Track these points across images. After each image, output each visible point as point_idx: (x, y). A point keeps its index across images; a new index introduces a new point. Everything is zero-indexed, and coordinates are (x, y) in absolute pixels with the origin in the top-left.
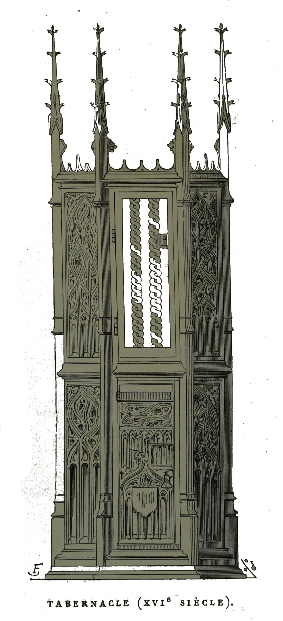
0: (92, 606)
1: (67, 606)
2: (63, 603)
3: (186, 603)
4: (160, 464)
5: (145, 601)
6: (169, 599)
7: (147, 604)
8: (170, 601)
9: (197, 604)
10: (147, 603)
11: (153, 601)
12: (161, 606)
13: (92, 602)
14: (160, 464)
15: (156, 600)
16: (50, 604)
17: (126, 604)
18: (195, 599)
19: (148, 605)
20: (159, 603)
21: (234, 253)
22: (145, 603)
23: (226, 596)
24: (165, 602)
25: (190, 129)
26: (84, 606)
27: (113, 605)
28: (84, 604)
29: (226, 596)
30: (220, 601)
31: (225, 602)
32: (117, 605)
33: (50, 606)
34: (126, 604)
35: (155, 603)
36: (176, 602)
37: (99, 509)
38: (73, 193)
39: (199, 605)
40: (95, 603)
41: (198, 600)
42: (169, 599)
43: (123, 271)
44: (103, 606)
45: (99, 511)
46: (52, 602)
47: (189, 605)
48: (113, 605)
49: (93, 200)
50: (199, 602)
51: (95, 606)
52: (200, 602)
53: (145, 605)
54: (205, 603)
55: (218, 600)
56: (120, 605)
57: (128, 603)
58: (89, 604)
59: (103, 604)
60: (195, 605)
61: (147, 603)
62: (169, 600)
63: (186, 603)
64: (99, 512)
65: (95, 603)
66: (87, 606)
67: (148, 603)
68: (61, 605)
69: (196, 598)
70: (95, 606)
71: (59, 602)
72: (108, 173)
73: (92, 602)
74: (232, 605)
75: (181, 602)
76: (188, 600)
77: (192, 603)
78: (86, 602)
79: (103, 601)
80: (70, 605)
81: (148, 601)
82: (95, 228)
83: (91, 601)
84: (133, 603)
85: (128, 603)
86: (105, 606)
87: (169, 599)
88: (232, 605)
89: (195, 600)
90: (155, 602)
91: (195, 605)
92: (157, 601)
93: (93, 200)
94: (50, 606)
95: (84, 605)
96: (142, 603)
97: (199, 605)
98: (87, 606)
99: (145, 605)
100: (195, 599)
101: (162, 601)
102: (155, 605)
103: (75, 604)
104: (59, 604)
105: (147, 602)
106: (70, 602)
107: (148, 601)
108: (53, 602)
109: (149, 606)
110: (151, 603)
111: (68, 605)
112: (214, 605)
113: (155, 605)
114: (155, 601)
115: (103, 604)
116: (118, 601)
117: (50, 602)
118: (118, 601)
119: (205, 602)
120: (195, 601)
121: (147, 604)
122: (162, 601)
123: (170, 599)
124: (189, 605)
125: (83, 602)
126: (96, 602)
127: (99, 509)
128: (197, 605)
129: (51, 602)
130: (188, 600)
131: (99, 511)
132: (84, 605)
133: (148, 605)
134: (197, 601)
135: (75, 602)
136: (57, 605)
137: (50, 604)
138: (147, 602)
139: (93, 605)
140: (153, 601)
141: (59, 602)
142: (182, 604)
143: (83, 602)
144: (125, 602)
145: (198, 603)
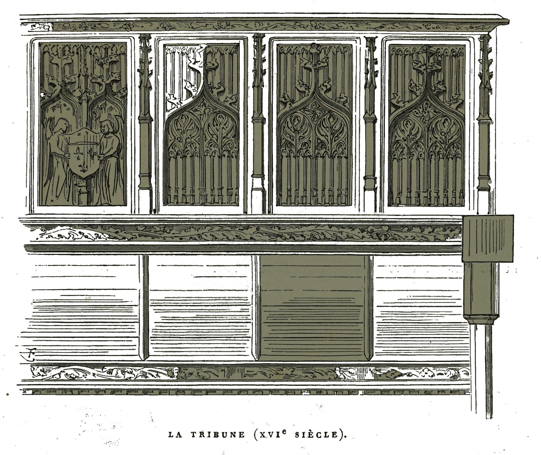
1: (215, 437)
3: (301, 435)
4: (375, 211)
5: (261, 433)
6: (284, 431)
7: (263, 436)
8: (286, 433)
9: (311, 436)
11: (269, 433)
12: (277, 437)
13: (232, 433)
14: (375, 211)
17: (242, 436)
18: (309, 431)
20: (275, 434)
23: (340, 429)
24: (281, 434)
27: (320, 437)
28: (233, 434)
29: (340, 429)
30: (334, 434)
31: (339, 434)
32: (325, 437)
33: (193, 436)
40: (234, 434)
41: (312, 433)
43: (254, 100)
50: (313, 435)
51: (235, 436)
52: (314, 435)
56: (328, 437)
61: (262, 435)
62: (284, 433)
63: (301, 435)
64: (449, 278)
65: (234, 434)
67: (264, 435)
68: (181, 436)
69: (310, 430)
70: (235, 436)
72: (194, 204)
73: (232, 433)
77: (307, 435)
79: (179, 433)
80: (218, 436)
82: (155, 312)
84: (249, 435)
85: (336, 434)
87: (284, 431)
88: (345, 437)
90: (271, 434)
92: (273, 432)
94: (193, 436)
95: (202, 436)
96: (258, 435)
97: (313, 437)
98: (204, 437)
100: (309, 431)
101: (278, 433)
102: (271, 436)
106: (218, 433)
108: (196, 433)
111: (216, 436)
112: (172, 436)
113: (271, 436)
116: (326, 433)
117: (193, 433)
118: (326, 433)
119: (319, 434)
120: (309, 433)
121: (263, 436)
122: (278, 433)
123: (285, 431)
124: (304, 437)
126: (235, 433)
129: (195, 433)
132: (202, 436)
134: (311, 433)
136: (201, 435)
140: (269, 433)
143: (215, 433)
144: (202, 434)
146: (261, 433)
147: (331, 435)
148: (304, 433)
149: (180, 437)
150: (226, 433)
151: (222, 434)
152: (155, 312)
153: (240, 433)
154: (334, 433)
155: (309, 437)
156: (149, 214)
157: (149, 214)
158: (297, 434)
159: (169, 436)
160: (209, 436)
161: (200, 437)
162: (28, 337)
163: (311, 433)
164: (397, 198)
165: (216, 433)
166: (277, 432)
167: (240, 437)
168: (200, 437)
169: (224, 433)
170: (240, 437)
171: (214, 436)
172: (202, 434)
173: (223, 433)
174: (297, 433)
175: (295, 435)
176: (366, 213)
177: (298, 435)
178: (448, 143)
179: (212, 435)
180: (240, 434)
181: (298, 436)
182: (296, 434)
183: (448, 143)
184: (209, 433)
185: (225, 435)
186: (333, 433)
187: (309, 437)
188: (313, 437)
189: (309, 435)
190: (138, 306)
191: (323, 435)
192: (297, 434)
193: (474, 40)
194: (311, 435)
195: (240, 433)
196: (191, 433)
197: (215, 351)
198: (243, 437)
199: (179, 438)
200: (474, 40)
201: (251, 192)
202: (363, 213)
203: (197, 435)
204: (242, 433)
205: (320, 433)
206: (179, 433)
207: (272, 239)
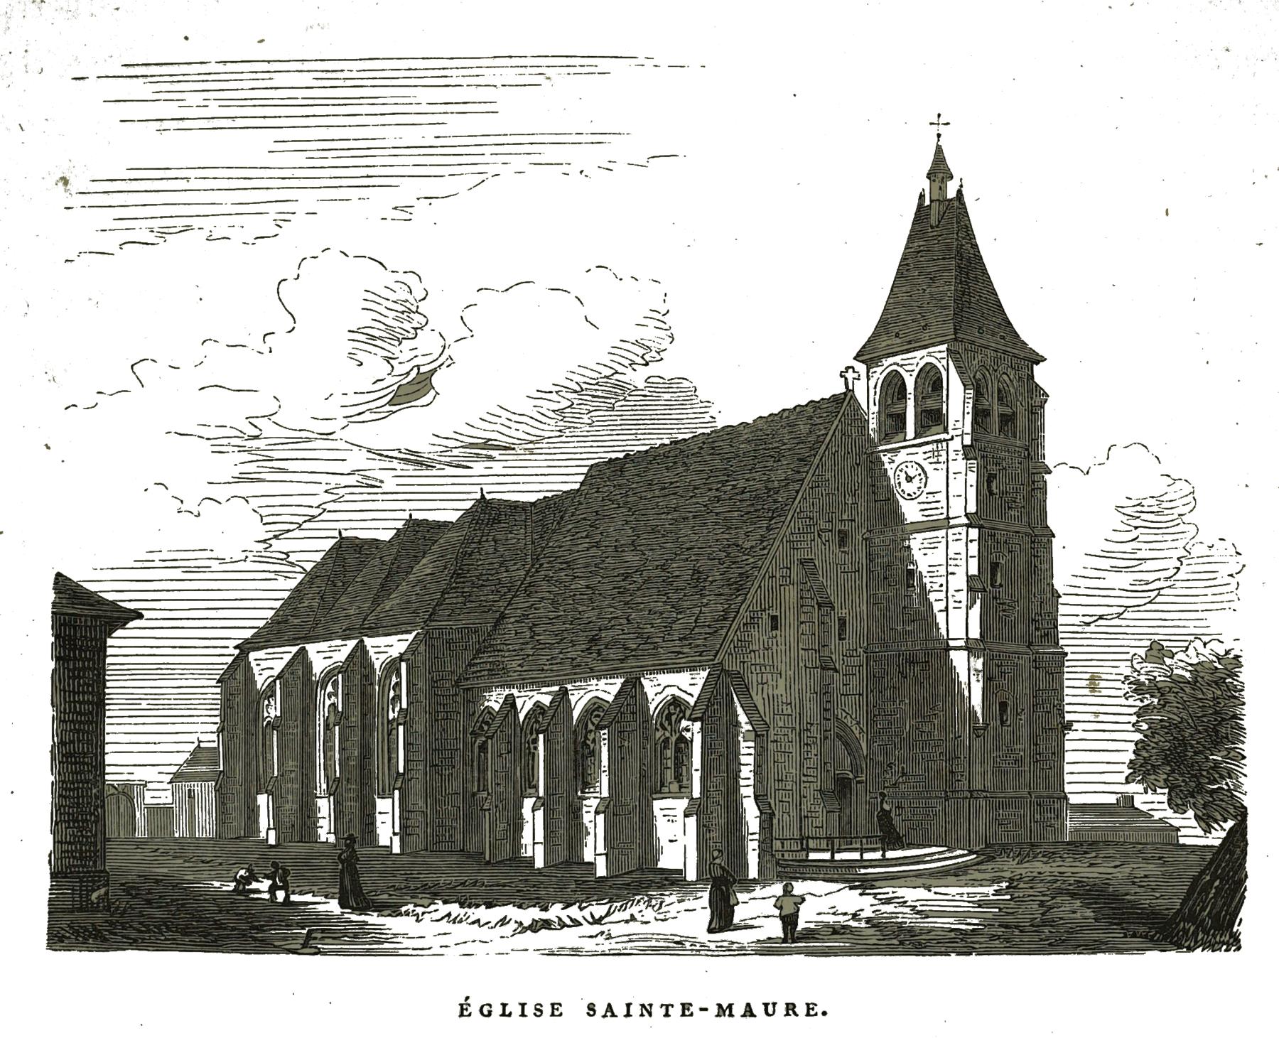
0: (642, 1015)
2: (758, 1009)
13: (643, 1006)
15: (771, 1002)
16: (667, 1010)
17: (687, 1013)
28: (791, 1008)
32: (503, 1015)
33: (667, 1015)
37: (294, 318)
39: (470, 1015)
44: (750, 1016)
45: (173, 434)
46: (672, 1006)
51: (650, 1014)
52: (474, 1009)
55: (682, 1004)
56: (510, 1015)
57: (815, 1007)
58: (801, 1009)
64: (176, 433)
65: (648, 1007)
66: (796, 1015)
70: (650, 1014)
71: (748, 1005)
73: (643, 1006)
78: (794, 1006)
79: (609, 1005)
83: (718, 1005)
85: (692, 1009)
86: (753, 1015)
95: (791, 1012)
98: (796, 1015)
104: (749, 1012)
109: (755, 1016)
115: (749, 1012)
116: (504, 1005)
117: (667, 1006)
118: (504, 1005)
120: (461, 1005)
126: (651, 1005)
127: (294, 318)
129: (670, 1007)
130: (520, 1004)
131: (173, 434)
132: (791, 1012)
137: (667, 1010)
139: (645, 1012)
141: (748, 1005)
142: (538, 1013)
144: (685, 1007)
149: (613, 1015)
150: (774, 1004)
151: (763, 1007)
153: (553, 1005)
154: (686, 1006)
155: (808, 1015)
156: (1135, 795)
157: (1135, 795)
158: (591, 1008)
159: (501, 1012)
161: (788, 1014)
162: (1107, 751)
163: (811, 1006)
164: (337, 531)
167: (553, 1015)
168: (788, 1014)
169: (769, 1004)
170: (553, 1015)
173: (766, 1005)
174: (591, 1006)
177: (595, 1011)
179: (635, 1010)
180: (808, 1009)
182: (536, 1009)
184: (523, 1005)
186: (683, 1005)
187: (808, 1015)
188: (470, 1015)
190: (482, 486)
191: (497, 1010)
192: (591, 1008)
194: (557, 1009)
195: (553, 1005)
196: (662, 1005)
197: (137, 655)
198: (561, 1015)
203: (676, 1011)
204: (556, 1007)
206: (609, 1005)
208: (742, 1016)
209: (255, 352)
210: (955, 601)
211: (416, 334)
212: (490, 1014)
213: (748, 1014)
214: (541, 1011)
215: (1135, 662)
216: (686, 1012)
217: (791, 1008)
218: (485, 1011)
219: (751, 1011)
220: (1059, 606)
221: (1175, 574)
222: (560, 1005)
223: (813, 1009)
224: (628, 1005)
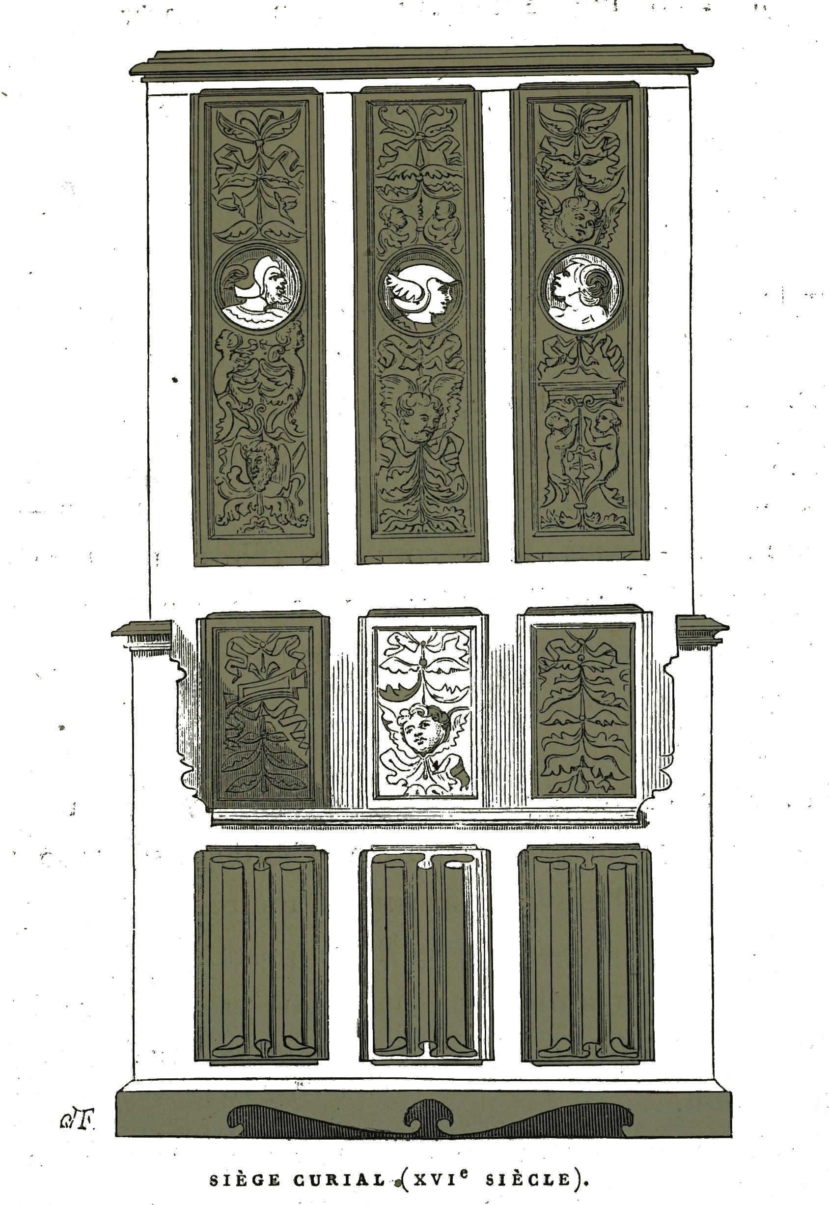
3: (221, 1180)
5: (417, 1176)
6: (464, 1173)
10: (420, 1180)
11: (434, 1175)
17: (564, 1182)
18: (239, 1174)
19: (424, 1184)
20: (445, 1180)
21: (62, 728)
22: (416, 1180)
24: (457, 1179)
25: (485, 421)
26: (331, 1184)
27: (537, 1184)
28: (332, 1179)
31: (573, 1179)
32: (546, 1183)
34: (564, 1180)
35: (437, 1179)
36: (477, 1177)
38: (536, 555)
39: (521, 1184)
41: (521, 1176)
42: (464, 1171)
44: (363, 1184)
47: (502, 1184)
48: (537, 1184)
49: (242, 668)
50: (245, 1180)
52: (525, 1179)
53: (417, 1184)
54: (534, 1180)
56: (552, 1183)
59: (240, 1182)
60: (515, 1184)
61: (420, 1180)
62: (464, 1175)
63: (221, 1180)
66: (336, 1184)
69: (240, 1171)
71: (362, 1175)
74: (586, 1183)
75: (488, 1179)
76: (545, 1175)
77: (508, 1180)
78: (334, 1177)
81: (423, 1175)
82: (338, 662)
84: (286, 1180)
86: (366, 1184)
87: (464, 1173)
88: (586, 1183)
89: (237, 1176)
90: (437, 1177)
91: (515, 1184)
92: (440, 1175)
93: (242, 668)
95: (331, 1182)
97: (521, 1184)
98: (336, 1184)
99: (417, 1184)
100: (239, 1174)
101: (451, 1176)
102: (437, 1183)
103: (515, 1179)
104: (362, 1181)
105: (420, 1177)
107: (423, 1175)
110: (428, 1179)
113: (437, 1183)
114: (436, 1175)
115: (362, 1181)
116: (547, 1176)
118: (547, 1176)
120: (239, 1177)
122: (451, 1176)
123: (466, 1172)
124: (502, 1184)
125: (328, 1175)
128: (242, 1185)
130: (345, 1175)
132: (331, 1182)
133: (424, 1184)
134: (241, 1178)
135: (517, 1176)
138: (420, 1177)
140: (434, 1175)
141: (362, 1175)
143: (328, 1175)
145: (567, 1180)
146: (417, 1176)
147: (557, 1181)
148: (502, 1176)
150: (319, 1176)
152: (338, 662)
153: (561, 1175)
160: (347, 1184)
161: (329, 1184)
163: (564, 1177)
165: (332, 1177)
166: (500, 1175)
167: (239, 1185)
169: (314, 1176)
170: (239, 1185)
171: (327, 1182)
172: (517, 1176)
173: (312, 1177)
175: (486, 1180)
176: (527, 807)
177: (217, 1182)
178: (468, 691)
180: (562, 1179)
181: (493, 1183)
183: (468, 691)
184: (347, 1176)
185: (316, 1179)
189: (239, 1180)
191: (542, 1179)
193: (465, 519)
195: (561, 1175)
199: (420, 1187)
200: (465, 519)
201: (457, 755)
202: (525, 807)
204: (564, 1177)
205: (536, 1176)
207: (629, 852)
208: (415, 1184)
209: (782, 289)
210: (438, 507)
211: (240, 517)
212: (261, 1183)
213: (362, 1183)
214: (491, 1180)
215: (592, 401)
216: (517, 1181)
217: (332, 1179)
218: (257, 1179)
219: (364, 1180)
220: (153, 619)
221: (258, 285)
222: (567, 1175)
223: (519, 1179)
224: (347, 1176)
